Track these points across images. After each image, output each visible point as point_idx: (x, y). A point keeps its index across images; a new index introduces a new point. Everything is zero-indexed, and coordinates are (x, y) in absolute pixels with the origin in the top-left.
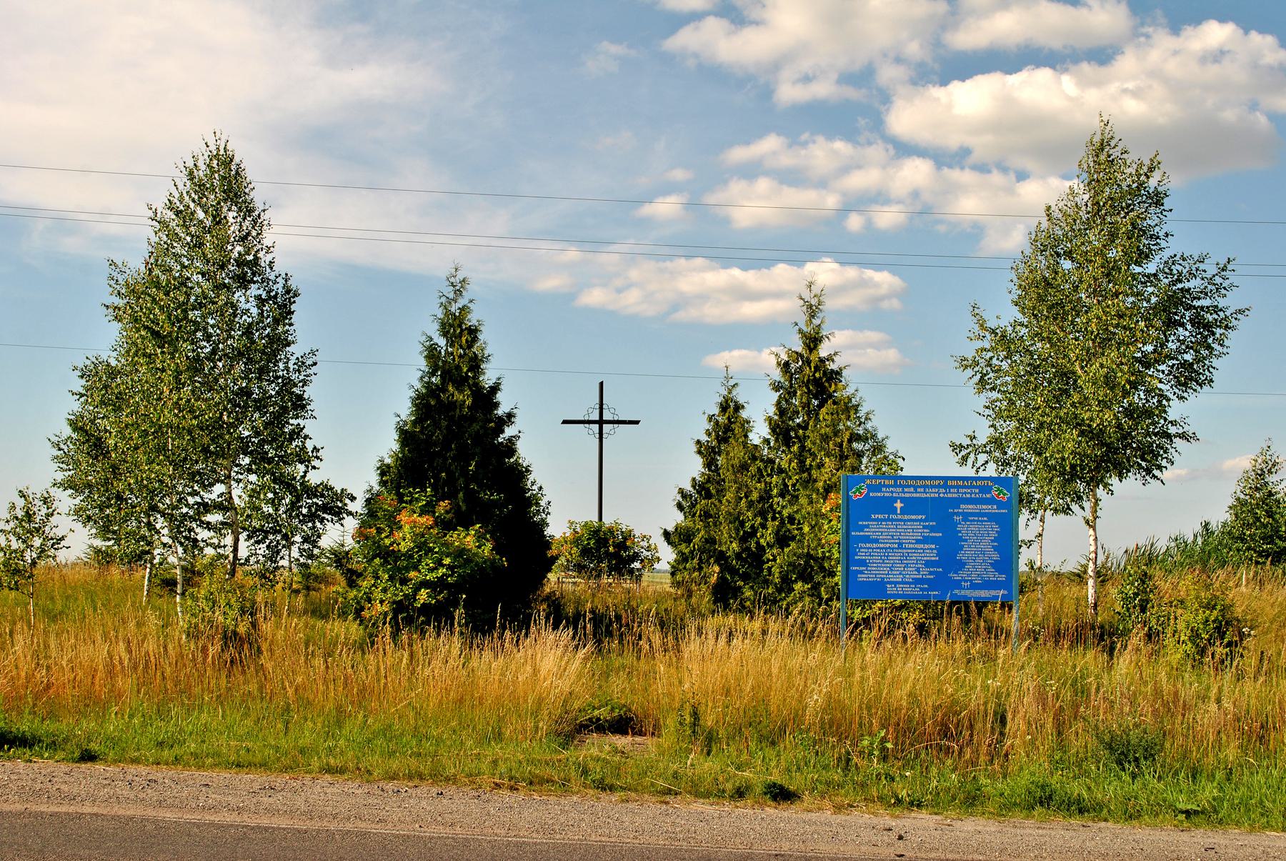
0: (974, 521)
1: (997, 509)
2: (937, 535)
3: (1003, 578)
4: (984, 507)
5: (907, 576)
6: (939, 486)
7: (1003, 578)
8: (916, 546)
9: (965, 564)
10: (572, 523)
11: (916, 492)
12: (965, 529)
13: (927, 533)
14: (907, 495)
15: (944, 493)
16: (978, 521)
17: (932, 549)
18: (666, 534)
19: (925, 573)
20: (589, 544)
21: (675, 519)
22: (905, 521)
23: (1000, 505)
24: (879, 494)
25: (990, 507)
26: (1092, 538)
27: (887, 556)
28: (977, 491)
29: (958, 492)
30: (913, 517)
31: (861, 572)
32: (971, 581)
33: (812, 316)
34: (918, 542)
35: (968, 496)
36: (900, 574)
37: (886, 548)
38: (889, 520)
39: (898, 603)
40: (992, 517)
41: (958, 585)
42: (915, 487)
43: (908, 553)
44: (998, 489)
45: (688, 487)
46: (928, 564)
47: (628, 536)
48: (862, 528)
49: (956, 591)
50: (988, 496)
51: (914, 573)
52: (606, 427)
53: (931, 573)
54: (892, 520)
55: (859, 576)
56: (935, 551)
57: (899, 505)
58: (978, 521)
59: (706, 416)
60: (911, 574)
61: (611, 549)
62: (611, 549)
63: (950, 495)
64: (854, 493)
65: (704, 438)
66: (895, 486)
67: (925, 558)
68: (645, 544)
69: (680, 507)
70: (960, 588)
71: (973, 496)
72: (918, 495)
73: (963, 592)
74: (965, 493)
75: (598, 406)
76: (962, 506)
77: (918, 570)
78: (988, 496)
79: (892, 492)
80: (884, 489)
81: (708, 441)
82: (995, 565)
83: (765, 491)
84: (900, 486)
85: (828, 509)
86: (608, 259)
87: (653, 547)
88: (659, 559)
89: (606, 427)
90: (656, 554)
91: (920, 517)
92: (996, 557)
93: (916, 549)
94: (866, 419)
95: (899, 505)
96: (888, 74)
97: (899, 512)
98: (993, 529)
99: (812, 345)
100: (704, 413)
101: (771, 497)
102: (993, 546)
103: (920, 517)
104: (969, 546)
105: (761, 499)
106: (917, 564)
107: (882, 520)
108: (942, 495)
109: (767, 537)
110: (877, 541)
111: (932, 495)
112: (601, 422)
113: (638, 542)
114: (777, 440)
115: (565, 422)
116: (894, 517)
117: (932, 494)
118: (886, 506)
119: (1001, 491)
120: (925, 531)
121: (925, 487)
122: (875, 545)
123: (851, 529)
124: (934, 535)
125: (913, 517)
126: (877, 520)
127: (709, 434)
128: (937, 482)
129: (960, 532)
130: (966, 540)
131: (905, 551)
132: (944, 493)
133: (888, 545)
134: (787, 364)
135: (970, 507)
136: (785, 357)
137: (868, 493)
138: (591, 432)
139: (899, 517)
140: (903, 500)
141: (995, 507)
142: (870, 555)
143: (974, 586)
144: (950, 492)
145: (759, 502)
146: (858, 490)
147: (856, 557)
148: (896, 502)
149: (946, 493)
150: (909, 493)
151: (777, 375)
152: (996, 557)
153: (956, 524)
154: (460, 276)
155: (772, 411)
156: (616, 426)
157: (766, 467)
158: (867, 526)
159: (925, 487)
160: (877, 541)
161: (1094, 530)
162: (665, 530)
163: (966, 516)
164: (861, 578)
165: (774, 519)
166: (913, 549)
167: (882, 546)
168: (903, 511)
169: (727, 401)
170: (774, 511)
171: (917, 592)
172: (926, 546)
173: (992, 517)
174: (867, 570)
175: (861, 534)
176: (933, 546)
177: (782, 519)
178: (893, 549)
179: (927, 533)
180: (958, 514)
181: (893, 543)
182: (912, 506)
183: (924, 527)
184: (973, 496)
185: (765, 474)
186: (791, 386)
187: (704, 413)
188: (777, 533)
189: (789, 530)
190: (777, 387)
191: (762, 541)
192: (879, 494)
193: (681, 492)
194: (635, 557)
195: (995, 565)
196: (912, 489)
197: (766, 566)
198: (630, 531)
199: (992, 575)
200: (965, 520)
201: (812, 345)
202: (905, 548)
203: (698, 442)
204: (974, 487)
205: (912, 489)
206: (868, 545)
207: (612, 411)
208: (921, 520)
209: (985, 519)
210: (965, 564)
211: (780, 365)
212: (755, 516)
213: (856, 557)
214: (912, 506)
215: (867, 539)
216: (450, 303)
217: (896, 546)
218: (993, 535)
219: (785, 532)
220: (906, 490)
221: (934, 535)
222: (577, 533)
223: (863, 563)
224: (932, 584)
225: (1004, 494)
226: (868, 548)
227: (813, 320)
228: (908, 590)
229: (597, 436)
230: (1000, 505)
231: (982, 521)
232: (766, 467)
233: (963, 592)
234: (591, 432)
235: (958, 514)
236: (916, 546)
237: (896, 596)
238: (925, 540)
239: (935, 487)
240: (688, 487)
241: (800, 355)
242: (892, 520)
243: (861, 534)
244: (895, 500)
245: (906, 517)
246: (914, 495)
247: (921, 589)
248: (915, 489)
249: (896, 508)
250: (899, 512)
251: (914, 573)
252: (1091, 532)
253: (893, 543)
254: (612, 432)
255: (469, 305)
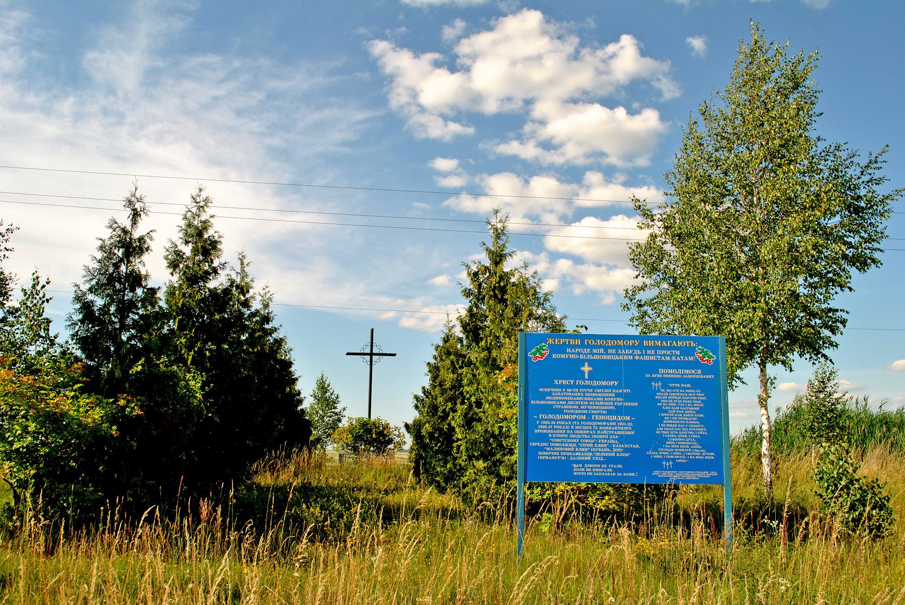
0: (675, 388)
1: (703, 373)
2: (633, 404)
3: (711, 456)
4: (687, 371)
5: (598, 454)
6: (633, 347)
7: (711, 456)
8: (608, 418)
9: (666, 439)
10: (350, 419)
11: (607, 354)
12: (666, 398)
13: (620, 401)
14: (596, 357)
15: (639, 355)
16: (680, 388)
17: (627, 422)
18: (407, 426)
19: (618, 450)
20: (359, 432)
21: (412, 416)
22: (594, 387)
23: (706, 370)
24: (563, 356)
25: (693, 372)
26: (765, 417)
27: (573, 430)
28: (678, 352)
29: (656, 354)
30: (604, 383)
31: (543, 449)
32: (674, 460)
33: (498, 237)
34: (610, 413)
35: (668, 358)
36: (589, 451)
37: (572, 420)
38: (574, 386)
39: (583, 485)
40: (696, 384)
41: (658, 464)
42: (606, 348)
43: (598, 426)
44: (702, 351)
45: (421, 394)
46: (622, 439)
47: (386, 427)
48: (543, 396)
49: (656, 473)
50: (691, 359)
51: (606, 450)
52: (368, 357)
53: (626, 450)
54: (579, 387)
55: (540, 453)
56: (630, 424)
57: (586, 369)
58: (680, 388)
59: (434, 347)
60: (602, 452)
61: (374, 436)
62: (374, 436)
63: (646, 358)
64: (534, 354)
65: (433, 361)
66: (582, 346)
67: (619, 433)
68: (396, 433)
69: (416, 407)
70: (661, 468)
71: (673, 358)
72: (609, 357)
73: (664, 474)
74: (664, 355)
75: (369, 344)
76: (661, 371)
77: (610, 446)
78: (691, 359)
79: (579, 354)
80: (568, 350)
81: (435, 363)
82: (701, 440)
83: (457, 380)
84: (588, 346)
85: (504, 379)
86: (417, 303)
87: (402, 434)
88: (405, 443)
89: (368, 357)
90: (404, 440)
91: (611, 383)
92: (702, 430)
93: (609, 421)
94: (545, 300)
95: (586, 369)
96: (550, 219)
97: (586, 377)
98: (698, 398)
99: (498, 260)
100: (432, 345)
101: (461, 386)
102: (699, 419)
103: (611, 383)
104: (671, 418)
105: (453, 387)
106: (609, 439)
107: (567, 387)
108: (637, 358)
109: (456, 420)
110: (560, 411)
111: (626, 358)
112: (371, 354)
113: (393, 431)
114: (467, 337)
115: (348, 354)
116: (582, 383)
117: (625, 356)
118: (572, 369)
119: (706, 353)
120: (618, 399)
121: (617, 347)
122: (559, 417)
123: (530, 396)
124: (628, 404)
125: (604, 383)
126: (561, 386)
127: (436, 358)
128: (631, 343)
129: (659, 401)
130: (666, 411)
131: (594, 423)
132: (639, 355)
133: (574, 417)
134: (476, 274)
135: (671, 371)
136: (474, 268)
137: (550, 355)
138: (365, 361)
139: (587, 383)
140: (591, 363)
141: (699, 371)
142: (553, 429)
143: (677, 467)
144: (646, 354)
145: (451, 390)
146: (538, 350)
147: (536, 431)
148: (583, 365)
149: (642, 355)
150: (598, 355)
151: (468, 284)
152: (702, 430)
153: (655, 392)
154: (204, 195)
155: (464, 313)
156: (381, 357)
157: (458, 360)
158: (550, 394)
159: (617, 347)
160: (560, 411)
161: (766, 409)
162: (406, 423)
163: (666, 382)
164: (543, 456)
165: (463, 403)
166: (603, 421)
167: (567, 417)
168: (592, 376)
169: (448, 337)
170: (464, 398)
171: (609, 473)
172: (620, 418)
173: (696, 384)
174: (549, 446)
175: (543, 402)
176: (628, 418)
177: (470, 404)
178: (580, 421)
179: (620, 401)
180: (656, 380)
181: (580, 414)
182: (602, 370)
183: (617, 395)
184: (673, 358)
185: (457, 366)
186: (479, 292)
187: (432, 345)
188: (466, 415)
189: (476, 413)
190: (467, 293)
191: (453, 423)
192: (563, 356)
193: (417, 398)
194: (390, 441)
195: (701, 440)
196: (602, 351)
197: (455, 445)
198: (387, 424)
199: (699, 453)
200: (665, 387)
201: (498, 260)
202: (595, 420)
203: (429, 364)
204: (676, 348)
205: (602, 351)
206: (550, 416)
207: (379, 347)
208: (613, 387)
209: (689, 385)
210: (666, 439)
211: (470, 275)
212: (447, 401)
213: (536, 431)
214: (602, 370)
215: (549, 409)
216: (194, 218)
217: (584, 417)
218: (699, 405)
219: (473, 414)
220: (595, 351)
221: (628, 404)
222: (352, 425)
223: (544, 438)
224: (627, 464)
225: (710, 357)
226: (551, 420)
227: (499, 241)
228: (599, 471)
229: (369, 363)
230: (706, 370)
231: (685, 388)
232: (458, 360)
233: (664, 474)
234: (365, 361)
235: (656, 380)
236: (608, 418)
237: (580, 479)
238: (618, 411)
239: (629, 347)
240: (421, 394)
241: (487, 268)
242: (579, 387)
243: (543, 402)
244: (582, 363)
245: (595, 383)
246: (605, 357)
247: (615, 470)
248: (606, 350)
249: (583, 372)
250: (586, 377)
251: (606, 450)
252: (763, 411)
253: (580, 414)
254: (378, 361)
255: (210, 220)
